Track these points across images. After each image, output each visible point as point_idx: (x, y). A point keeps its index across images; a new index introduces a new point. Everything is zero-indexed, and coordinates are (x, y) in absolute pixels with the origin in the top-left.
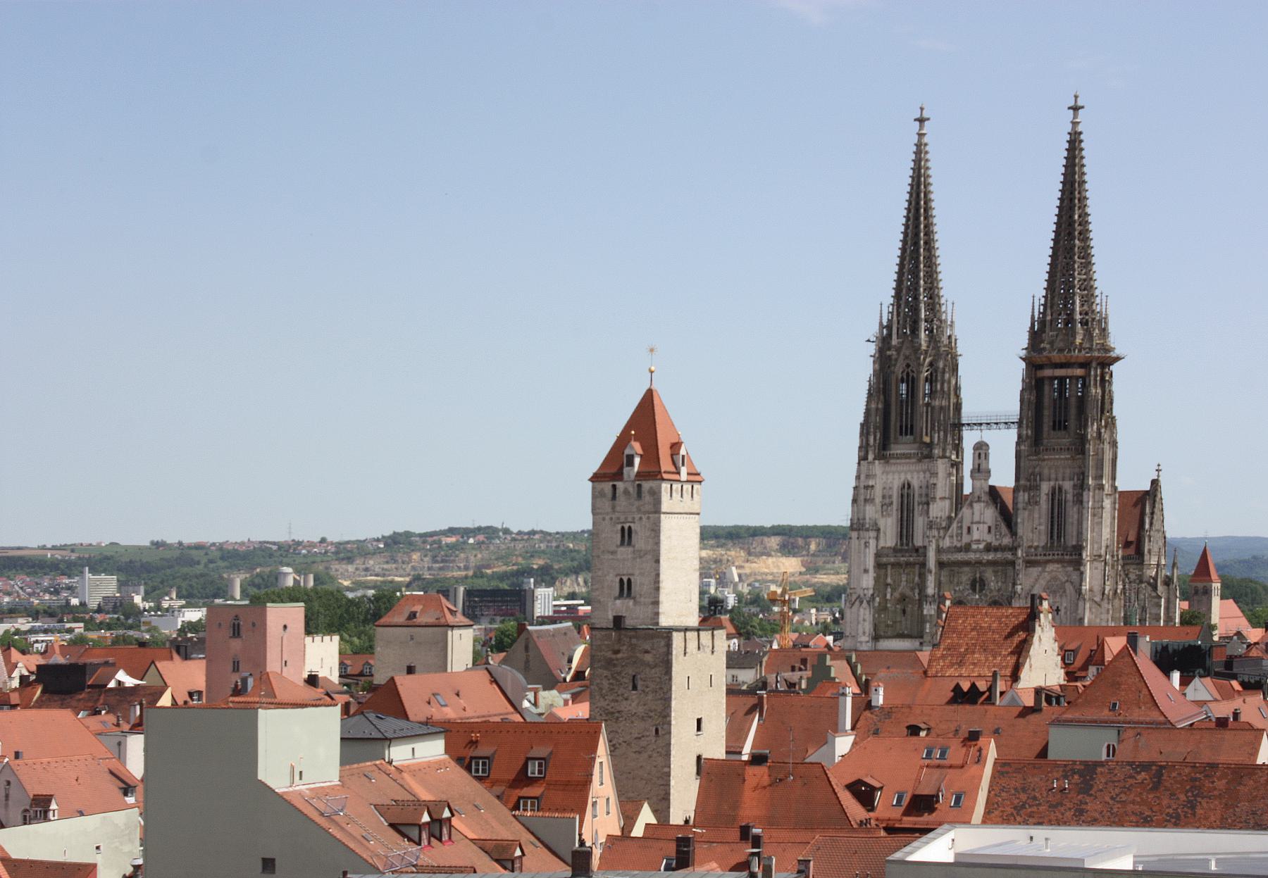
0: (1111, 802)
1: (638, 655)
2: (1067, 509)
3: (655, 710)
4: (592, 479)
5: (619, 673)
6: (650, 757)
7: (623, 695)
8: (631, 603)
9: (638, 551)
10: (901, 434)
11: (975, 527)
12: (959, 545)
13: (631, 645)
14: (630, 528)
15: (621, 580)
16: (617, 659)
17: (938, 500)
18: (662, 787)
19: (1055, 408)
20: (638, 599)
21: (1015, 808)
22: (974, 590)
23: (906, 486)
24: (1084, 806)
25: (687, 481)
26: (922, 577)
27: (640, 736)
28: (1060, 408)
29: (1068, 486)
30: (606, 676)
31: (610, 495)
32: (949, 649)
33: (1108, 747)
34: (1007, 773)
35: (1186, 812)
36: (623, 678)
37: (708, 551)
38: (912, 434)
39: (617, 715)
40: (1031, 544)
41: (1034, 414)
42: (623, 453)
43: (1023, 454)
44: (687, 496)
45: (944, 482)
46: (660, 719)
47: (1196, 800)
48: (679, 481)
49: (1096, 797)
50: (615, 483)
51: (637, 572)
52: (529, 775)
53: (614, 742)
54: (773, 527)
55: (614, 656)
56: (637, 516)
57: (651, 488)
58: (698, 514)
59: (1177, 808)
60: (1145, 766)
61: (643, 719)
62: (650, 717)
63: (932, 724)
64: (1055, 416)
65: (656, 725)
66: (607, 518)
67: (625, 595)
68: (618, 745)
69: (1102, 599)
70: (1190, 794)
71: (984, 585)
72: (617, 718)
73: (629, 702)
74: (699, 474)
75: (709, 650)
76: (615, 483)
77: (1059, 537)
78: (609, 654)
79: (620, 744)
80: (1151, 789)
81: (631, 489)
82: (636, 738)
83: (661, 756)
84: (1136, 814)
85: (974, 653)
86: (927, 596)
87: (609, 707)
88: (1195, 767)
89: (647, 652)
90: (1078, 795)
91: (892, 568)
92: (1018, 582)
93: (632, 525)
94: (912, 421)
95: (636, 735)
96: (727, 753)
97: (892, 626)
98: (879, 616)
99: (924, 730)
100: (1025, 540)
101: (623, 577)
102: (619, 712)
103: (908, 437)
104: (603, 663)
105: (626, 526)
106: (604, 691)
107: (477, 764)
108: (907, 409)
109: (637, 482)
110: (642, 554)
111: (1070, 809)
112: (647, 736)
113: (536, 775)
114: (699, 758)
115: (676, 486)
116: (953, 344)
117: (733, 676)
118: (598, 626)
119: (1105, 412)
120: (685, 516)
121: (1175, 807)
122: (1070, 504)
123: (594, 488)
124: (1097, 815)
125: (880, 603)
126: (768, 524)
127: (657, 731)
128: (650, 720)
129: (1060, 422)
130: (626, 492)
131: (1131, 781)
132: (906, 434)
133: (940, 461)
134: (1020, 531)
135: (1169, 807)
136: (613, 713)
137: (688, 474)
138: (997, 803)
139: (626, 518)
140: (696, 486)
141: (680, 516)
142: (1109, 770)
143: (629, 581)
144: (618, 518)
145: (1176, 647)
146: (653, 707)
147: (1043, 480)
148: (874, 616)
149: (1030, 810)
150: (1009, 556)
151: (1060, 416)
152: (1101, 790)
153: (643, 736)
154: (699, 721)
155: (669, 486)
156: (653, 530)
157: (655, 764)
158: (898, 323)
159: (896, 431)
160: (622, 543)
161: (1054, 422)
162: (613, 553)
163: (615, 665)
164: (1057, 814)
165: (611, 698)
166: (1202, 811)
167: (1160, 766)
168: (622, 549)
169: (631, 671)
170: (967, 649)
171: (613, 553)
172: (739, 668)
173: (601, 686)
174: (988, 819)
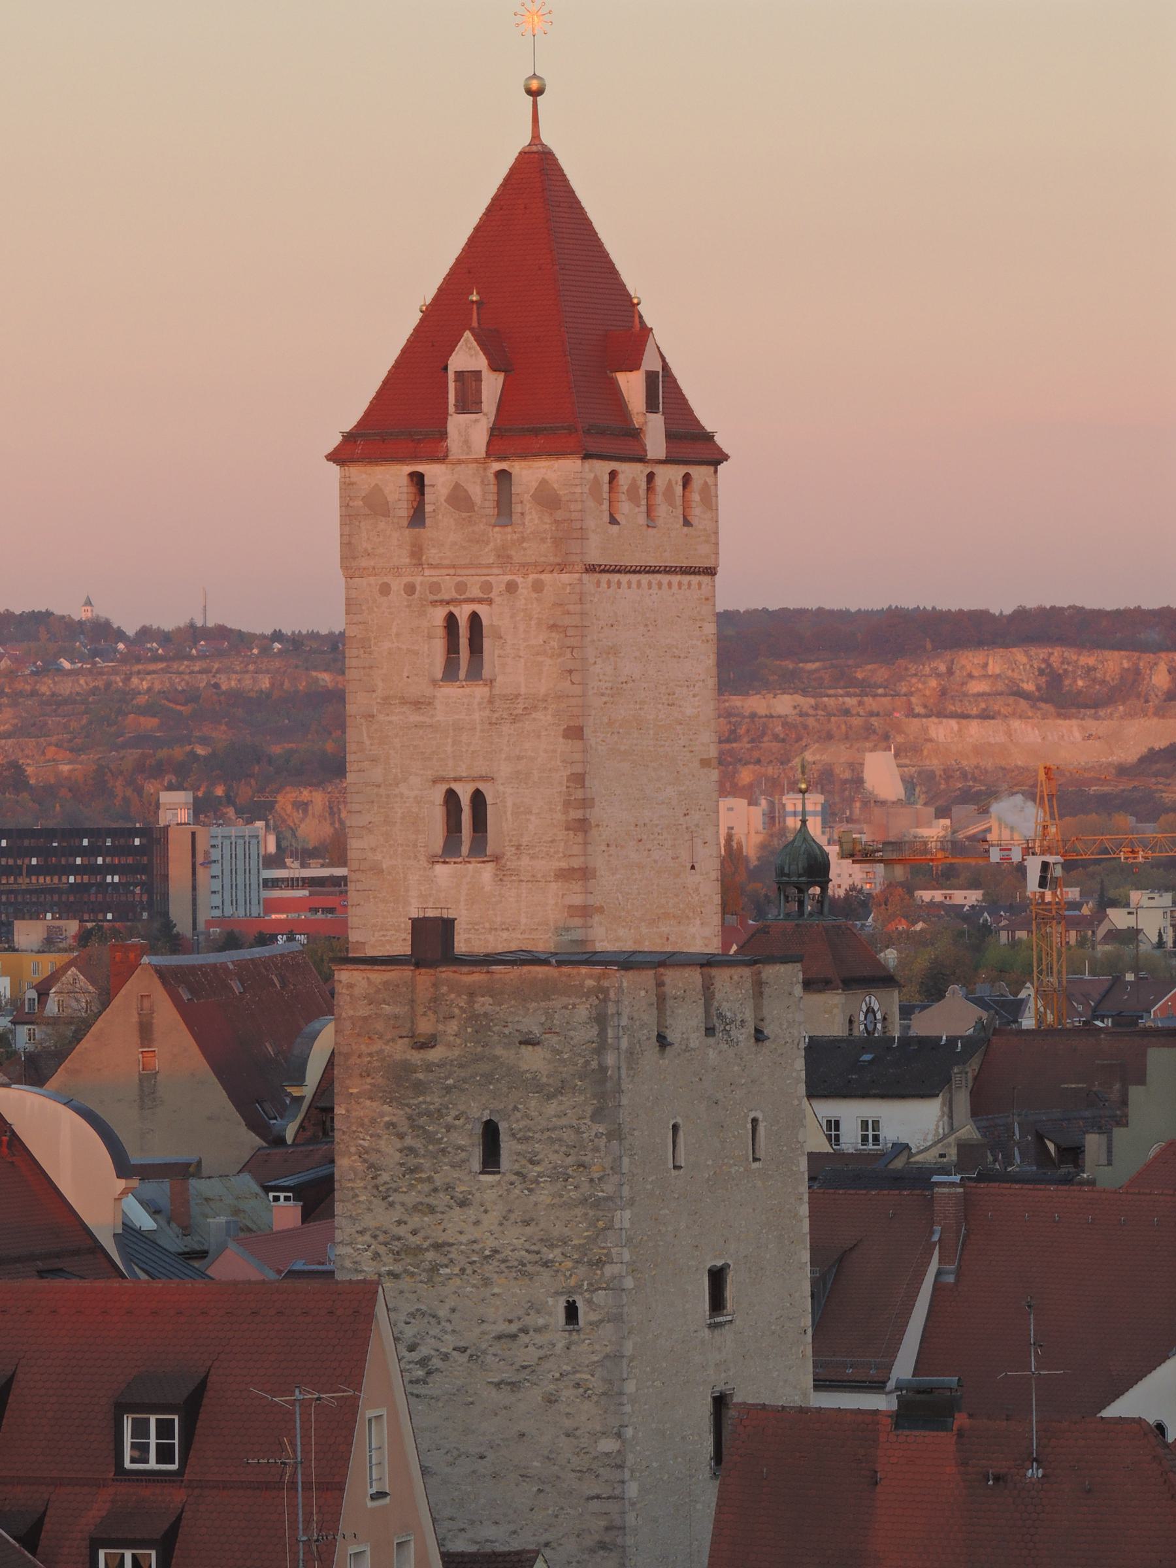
1: (499, 1051)
3: (565, 1241)
4: (336, 457)
7: (449, 1188)
8: (487, 872)
9: (505, 698)
13: (474, 1017)
14: (475, 618)
15: (451, 798)
16: (429, 1067)
18: (595, 1506)
27: (514, 1328)
30: (391, 1125)
31: (403, 511)
36: (449, 1128)
37: (799, 699)
39: (430, 1255)
42: (446, 368)
46: (582, 1270)
50: (420, 468)
51: (504, 770)
52: (128, 1465)
53: (424, 1351)
54: (1021, 615)
55: (416, 1057)
56: (499, 580)
57: (544, 483)
61: (522, 1271)
62: (546, 1264)
65: (570, 1292)
66: (397, 585)
67: (465, 849)
68: (436, 1362)
72: (434, 1269)
73: (471, 1213)
75: (744, 1035)
76: (420, 468)
78: (400, 1051)
79: (445, 1357)
81: (475, 491)
82: (499, 1338)
83: (586, 1396)
87: (402, 1231)
89: (529, 1041)
93: (482, 610)
101: (457, 787)
102: (437, 1246)
105: (463, 614)
106: (385, 1177)
107: (140, 1429)
109: (497, 466)
112: (538, 1330)
113: (152, 1465)
114: (720, 1402)
115: (630, 472)
117: (865, 1124)
118: (370, 952)
123: (346, 486)
126: (1002, 605)
127: (572, 1312)
130: (459, 499)
136: (419, 1250)
137: (670, 436)
139: (461, 587)
141: (645, 578)
143: (478, 799)
144: (435, 588)
153: (525, 1330)
154: (717, 1277)
156: (553, 627)
157: (568, 1423)
160: (450, 672)
162: (418, 704)
163: (419, 1088)
165: (412, 1198)
168: (450, 691)
169: (478, 1110)
171: (418, 704)
172: (883, 1096)
173: (373, 1158)
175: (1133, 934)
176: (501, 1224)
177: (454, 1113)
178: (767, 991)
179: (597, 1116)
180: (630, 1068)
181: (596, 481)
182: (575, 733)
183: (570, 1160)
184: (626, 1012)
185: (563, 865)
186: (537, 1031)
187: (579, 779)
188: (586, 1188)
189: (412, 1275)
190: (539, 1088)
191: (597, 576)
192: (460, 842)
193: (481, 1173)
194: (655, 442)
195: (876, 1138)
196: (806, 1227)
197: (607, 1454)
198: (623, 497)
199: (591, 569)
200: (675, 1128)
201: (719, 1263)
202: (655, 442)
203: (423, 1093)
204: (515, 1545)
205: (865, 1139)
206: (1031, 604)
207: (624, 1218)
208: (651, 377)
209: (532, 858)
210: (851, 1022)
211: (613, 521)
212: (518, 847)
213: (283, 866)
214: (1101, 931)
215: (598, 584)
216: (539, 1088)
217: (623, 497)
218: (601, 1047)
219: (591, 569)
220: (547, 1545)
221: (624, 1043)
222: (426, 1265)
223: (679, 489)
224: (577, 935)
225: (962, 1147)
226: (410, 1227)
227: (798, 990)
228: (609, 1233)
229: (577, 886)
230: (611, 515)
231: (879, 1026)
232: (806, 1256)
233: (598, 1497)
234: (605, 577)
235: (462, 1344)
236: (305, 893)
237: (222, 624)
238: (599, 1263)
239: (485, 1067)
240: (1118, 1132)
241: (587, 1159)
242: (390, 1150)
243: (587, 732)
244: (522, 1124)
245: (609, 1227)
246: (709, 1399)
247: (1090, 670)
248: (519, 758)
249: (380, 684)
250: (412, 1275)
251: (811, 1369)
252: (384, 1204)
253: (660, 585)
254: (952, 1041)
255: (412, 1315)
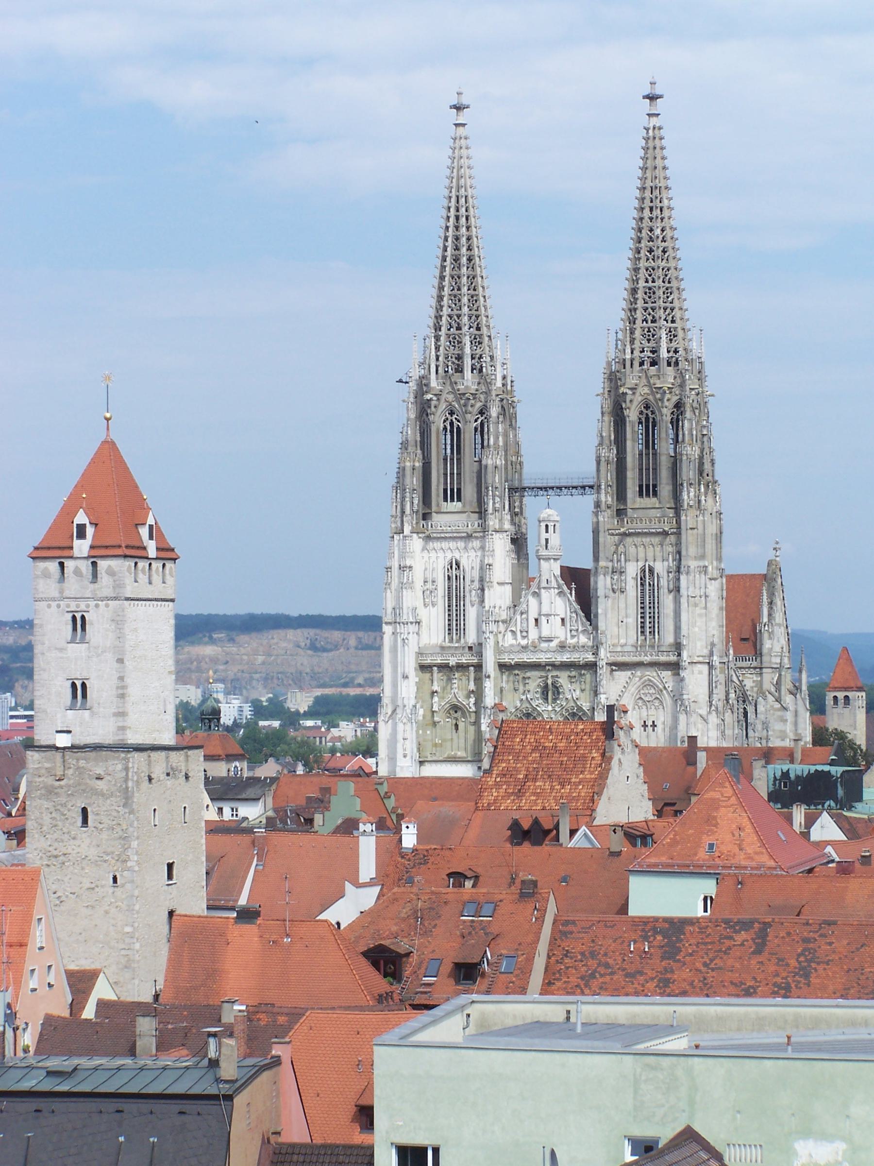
0: (704, 969)
1: (88, 781)
2: (661, 598)
3: (113, 853)
5: (64, 805)
6: (107, 912)
8: (87, 713)
10: (446, 500)
11: (543, 620)
12: (524, 642)
16: (61, 787)
17: (495, 584)
18: (123, 952)
19: (641, 470)
20: (95, 710)
21: (582, 978)
22: (546, 699)
23: (454, 566)
24: (669, 976)
25: (157, 558)
26: (479, 681)
27: (93, 886)
28: (648, 469)
29: (660, 568)
32: (505, 775)
33: (705, 899)
34: (571, 933)
35: (799, 982)
38: (459, 500)
39: (62, 858)
40: (616, 641)
41: (614, 477)
42: (73, 522)
43: (601, 529)
44: (157, 579)
45: (503, 561)
46: (119, 864)
47: (810, 966)
48: (147, 558)
49: (685, 964)
57: (110, 566)
58: (172, 600)
59: (788, 976)
60: (746, 925)
61: (96, 863)
62: (105, 861)
63: (479, 870)
64: (641, 479)
69: (710, 713)
70: (802, 959)
71: (559, 693)
73: (77, 842)
74: (173, 550)
77: (652, 633)
78: (50, 781)
80: (753, 953)
82: (88, 889)
84: (735, 985)
85: (535, 780)
86: (485, 708)
87: (51, 849)
88: (807, 924)
90: (661, 961)
91: (439, 672)
92: (602, 690)
94: (459, 483)
95: (88, 885)
96: (209, 908)
97: (441, 745)
98: (424, 732)
99: (470, 878)
100: (608, 637)
103: (455, 503)
104: (43, 792)
106: (45, 828)
108: (452, 469)
110: (100, 652)
111: (652, 979)
112: (102, 886)
114: (171, 913)
115: (142, 564)
116: (509, 388)
119: (705, 475)
120: (155, 603)
121: (784, 974)
122: (664, 591)
124: (685, 986)
125: (424, 716)
126: (294, 613)
127: (115, 879)
128: (105, 865)
129: (648, 486)
131: (728, 943)
132: (452, 500)
133: (497, 536)
134: (601, 625)
135: (777, 975)
136: (56, 857)
137: (158, 549)
138: (559, 971)
140: (169, 565)
141: (148, 603)
142: (700, 928)
143: (84, 685)
144: (68, 606)
145: (800, 774)
146: (109, 850)
147: (629, 560)
148: (417, 732)
149: (601, 980)
150: (590, 658)
151: (648, 479)
152: (691, 955)
154: (170, 866)
155: (147, 565)
158: (437, 359)
159: (438, 495)
161: (641, 487)
162: (61, 650)
164: (636, 986)
165: (56, 836)
166: (818, 981)
167: (764, 923)
170: (526, 775)
171: (61, 650)
173: (40, 821)
174: (547, 987)
175: (340, 738)
176: (88, 846)
177: (70, 805)
178: (189, 758)
179: (125, 805)
180: (137, 788)
181: (130, 566)
182: (120, 661)
183: (114, 823)
184: (136, 766)
185: (116, 711)
186: (102, 773)
187: (121, 678)
188: (120, 833)
189: (55, 865)
190: (103, 795)
191: (129, 602)
192: (77, 702)
193: (82, 827)
194: (152, 552)
195: (237, 815)
196: (204, 847)
197: (128, 933)
198: (140, 572)
199: (127, 599)
200: (155, 810)
201: (171, 862)
202: (152, 552)
203: (59, 797)
204: (93, 967)
205: (233, 815)
206: (304, 613)
207: (135, 844)
208: (151, 527)
209: (104, 708)
210: (229, 771)
211: (136, 581)
212: (99, 704)
213: (17, 710)
214: (328, 738)
215: (130, 605)
216: (103, 795)
217: (140, 572)
218: (126, 779)
219: (127, 599)
220: (105, 967)
221: (135, 778)
222: (60, 861)
223: (161, 569)
224: (121, 737)
225: (268, 819)
226: (54, 847)
227: (202, 759)
228: (129, 850)
229: (121, 719)
230: (163, 579)
231: (239, 773)
232: (204, 859)
233: (125, 949)
234: (133, 602)
235: (73, 891)
236: (25, 721)
237: (287, 614)
238: (125, 861)
239: (83, 787)
240: (326, 813)
241: (121, 822)
242: (47, 819)
243: (125, 661)
244: (97, 809)
245: (129, 847)
246: (167, 913)
247: (326, 638)
248: (100, 670)
249: (47, 642)
250: (55, 865)
251: (205, 901)
252: (44, 838)
253: (153, 605)
254: (266, 778)
255: (55, 880)
